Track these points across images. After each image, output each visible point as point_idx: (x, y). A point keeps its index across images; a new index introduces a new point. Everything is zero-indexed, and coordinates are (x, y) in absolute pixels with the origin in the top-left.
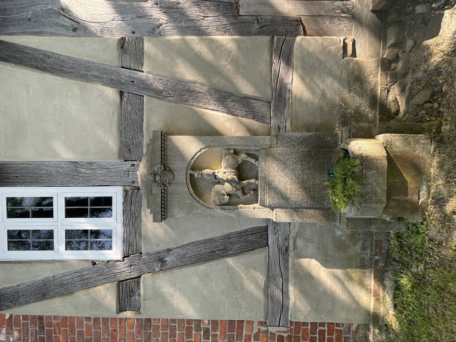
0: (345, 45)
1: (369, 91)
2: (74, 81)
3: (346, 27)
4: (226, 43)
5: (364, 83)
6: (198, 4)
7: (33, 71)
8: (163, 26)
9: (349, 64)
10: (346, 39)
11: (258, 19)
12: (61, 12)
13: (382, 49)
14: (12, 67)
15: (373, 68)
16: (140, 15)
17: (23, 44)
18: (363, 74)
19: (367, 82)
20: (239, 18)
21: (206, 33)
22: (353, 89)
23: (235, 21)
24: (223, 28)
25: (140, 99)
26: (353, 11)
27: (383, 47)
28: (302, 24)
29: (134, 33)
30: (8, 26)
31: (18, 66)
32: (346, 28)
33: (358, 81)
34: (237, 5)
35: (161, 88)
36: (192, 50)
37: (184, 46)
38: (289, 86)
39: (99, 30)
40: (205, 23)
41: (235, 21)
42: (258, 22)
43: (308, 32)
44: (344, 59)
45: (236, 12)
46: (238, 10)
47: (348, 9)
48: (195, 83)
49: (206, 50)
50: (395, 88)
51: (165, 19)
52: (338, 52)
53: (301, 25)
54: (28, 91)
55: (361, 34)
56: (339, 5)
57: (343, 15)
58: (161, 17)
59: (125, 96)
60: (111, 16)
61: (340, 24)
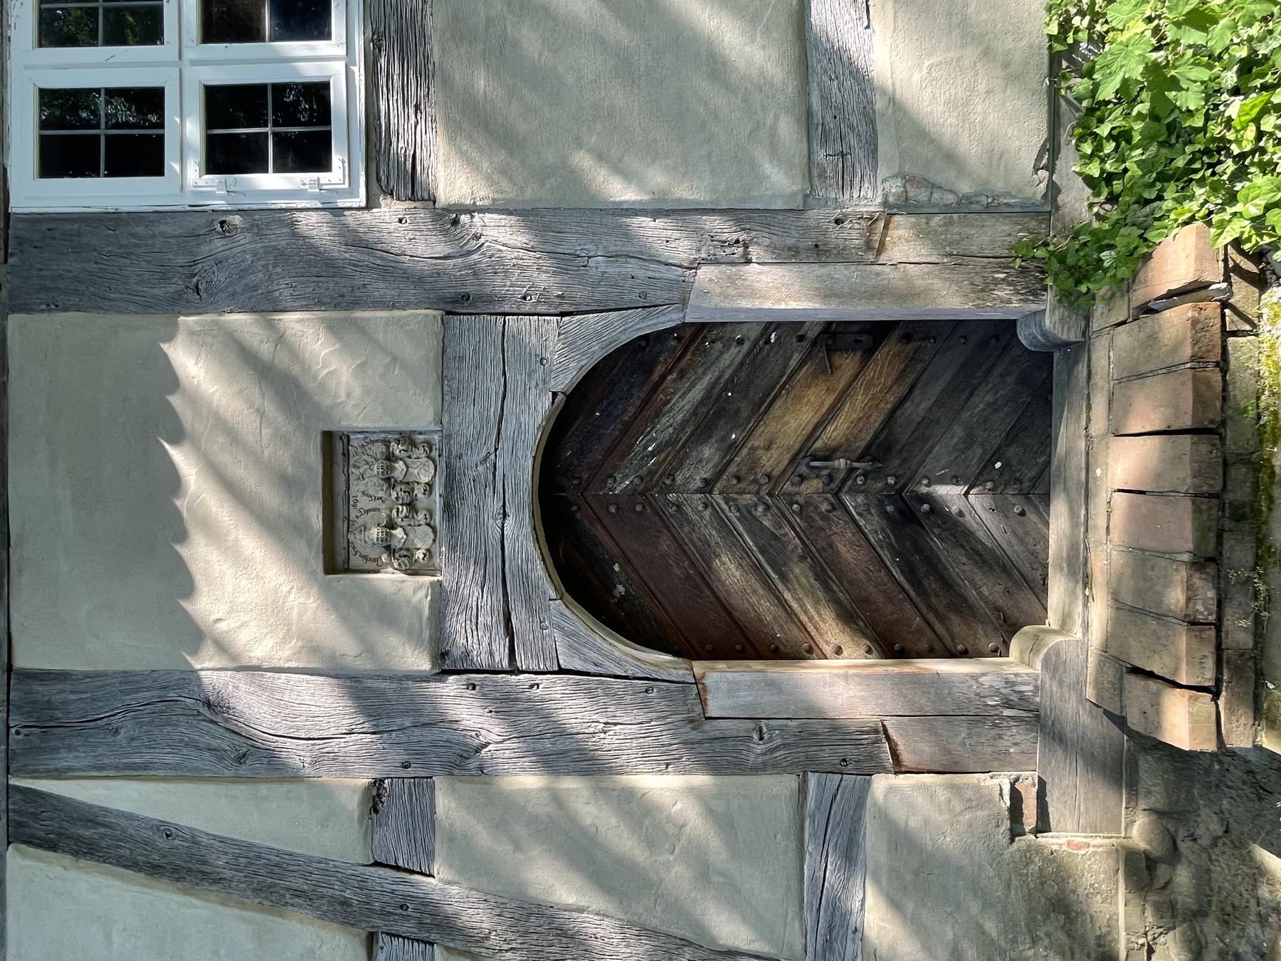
0: (1016, 797)
1: (1092, 941)
2: (236, 912)
3: (1015, 744)
4: (669, 801)
5: (1076, 917)
6: (590, 689)
7: (121, 878)
8: (490, 747)
9: (1029, 862)
10: (1017, 780)
11: (761, 730)
12: (204, 710)
13: (1127, 808)
14: (65, 868)
15: (1102, 876)
16: (426, 720)
17: (96, 803)
18: (1074, 892)
19: (1084, 914)
20: (708, 726)
21: (611, 767)
22: (1042, 935)
23: (695, 735)
24: (664, 754)
25: (424, 954)
26: (1038, 699)
27: (1128, 803)
28: (888, 738)
29: (406, 766)
30: (55, 750)
31: (83, 863)
32: (1018, 747)
33: (1059, 913)
34: (700, 686)
35: (484, 925)
36: (573, 820)
37: (546, 809)
38: (853, 919)
39: (308, 760)
40: (610, 741)
41: (695, 735)
42: (761, 739)
43: (907, 758)
44: (1015, 845)
45: (698, 709)
46: (703, 703)
47: (1022, 697)
48: (581, 910)
49: (613, 821)
50: (1171, 944)
51: (497, 730)
52: (997, 826)
53: (884, 740)
54: (108, 936)
55: (1062, 765)
56: (995, 684)
57: (1007, 712)
58: (486, 726)
59: (382, 948)
60: (344, 722)
61: (1000, 737)
